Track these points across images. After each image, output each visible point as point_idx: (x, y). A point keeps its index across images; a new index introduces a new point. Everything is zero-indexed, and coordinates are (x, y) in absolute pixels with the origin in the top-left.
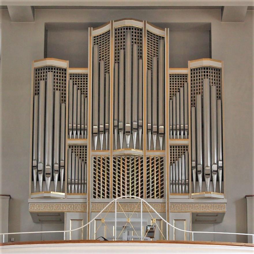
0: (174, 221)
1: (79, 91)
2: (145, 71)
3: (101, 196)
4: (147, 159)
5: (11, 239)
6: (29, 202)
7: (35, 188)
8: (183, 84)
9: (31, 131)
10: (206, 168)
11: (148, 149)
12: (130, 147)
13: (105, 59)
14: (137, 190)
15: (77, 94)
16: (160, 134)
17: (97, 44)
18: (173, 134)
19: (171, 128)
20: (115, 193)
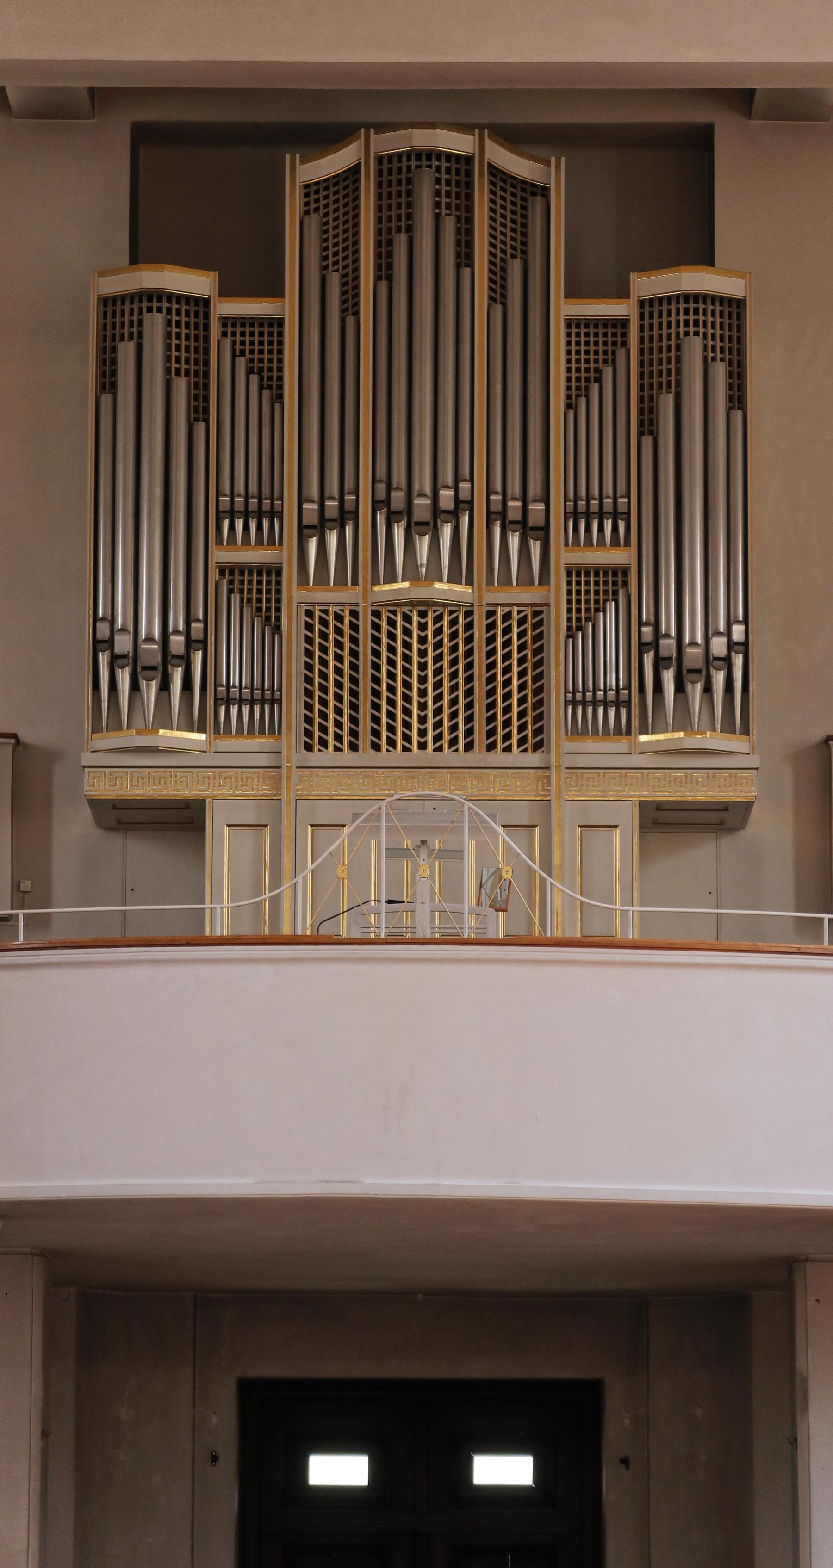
0: (578, 830)
1: (254, 379)
2: (481, 305)
3: (331, 742)
4: (487, 618)
5: (22, 884)
6: (84, 764)
7: (105, 714)
8: (614, 353)
9: (88, 546)
10: (689, 651)
11: (490, 583)
12: (425, 576)
13: (341, 264)
14: (453, 722)
15: (248, 388)
16: (532, 529)
17: (316, 210)
18: (576, 529)
19: (570, 508)
20: (376, 733)
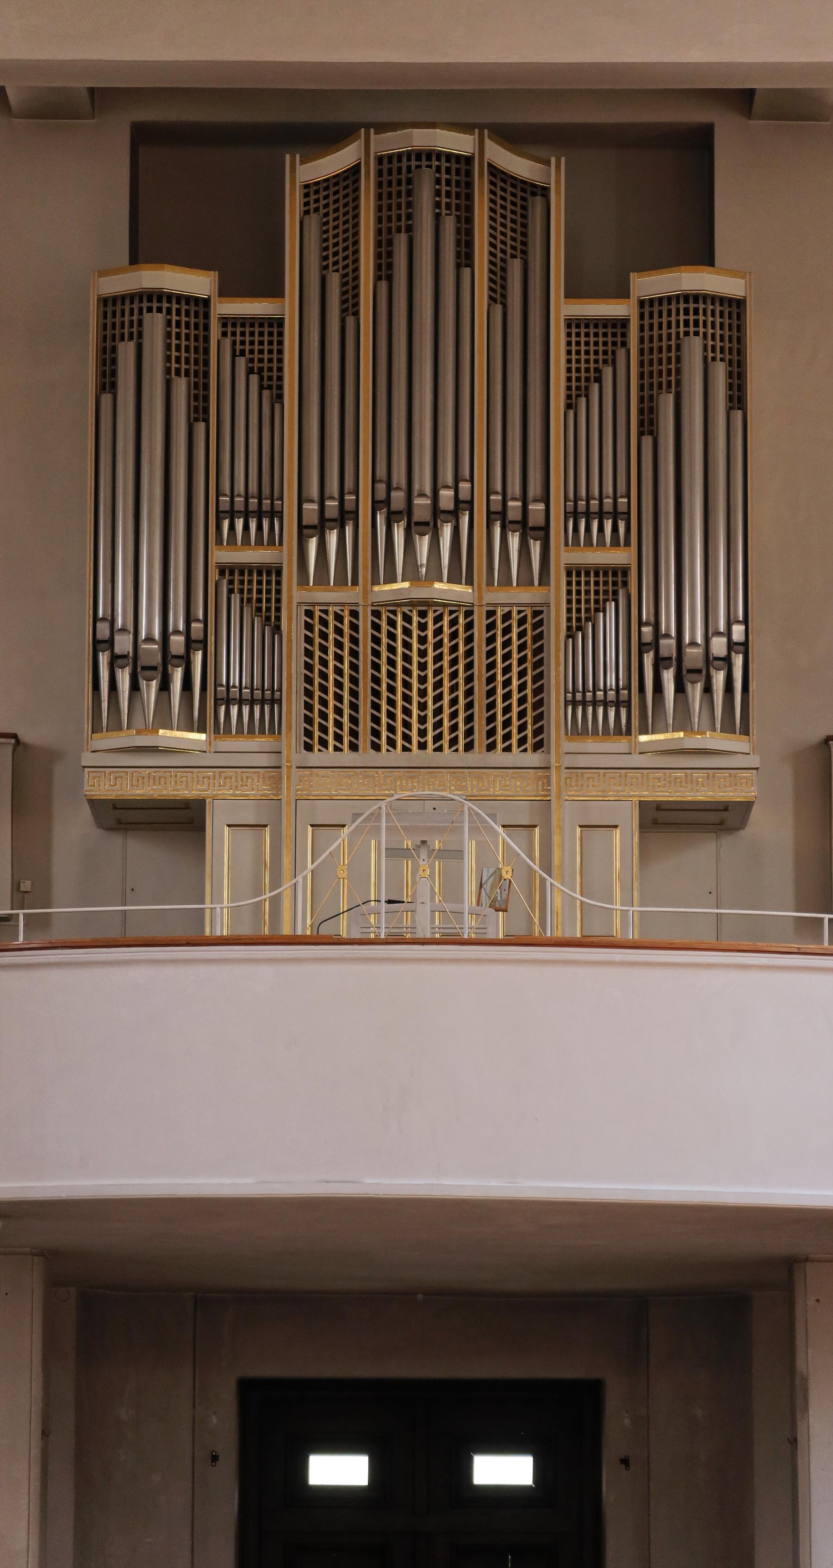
0: (578, 830)
1: (254, 379)
2: (481, 305)
3: (331, 742)
4: (487, 618)
5: (22, 884)
6: (84, 764)
7: (105, 714)
8: (614, 353)
9: (88, 546)
10: (689, 651)
11: (490, 583)
12: (425, 576)
13: (341, 264)
14: (453, 722)
15: (248, 388)
16: (532, 529)
17: (316, 210)
18: (576, 529)
19: (570, 508)
20: (376, 733)
